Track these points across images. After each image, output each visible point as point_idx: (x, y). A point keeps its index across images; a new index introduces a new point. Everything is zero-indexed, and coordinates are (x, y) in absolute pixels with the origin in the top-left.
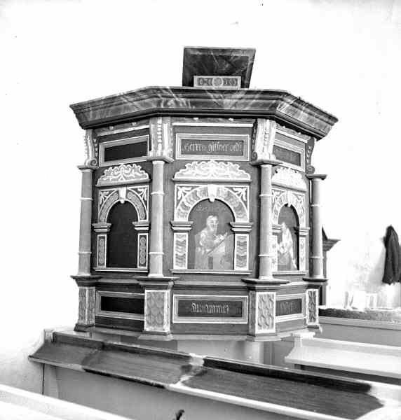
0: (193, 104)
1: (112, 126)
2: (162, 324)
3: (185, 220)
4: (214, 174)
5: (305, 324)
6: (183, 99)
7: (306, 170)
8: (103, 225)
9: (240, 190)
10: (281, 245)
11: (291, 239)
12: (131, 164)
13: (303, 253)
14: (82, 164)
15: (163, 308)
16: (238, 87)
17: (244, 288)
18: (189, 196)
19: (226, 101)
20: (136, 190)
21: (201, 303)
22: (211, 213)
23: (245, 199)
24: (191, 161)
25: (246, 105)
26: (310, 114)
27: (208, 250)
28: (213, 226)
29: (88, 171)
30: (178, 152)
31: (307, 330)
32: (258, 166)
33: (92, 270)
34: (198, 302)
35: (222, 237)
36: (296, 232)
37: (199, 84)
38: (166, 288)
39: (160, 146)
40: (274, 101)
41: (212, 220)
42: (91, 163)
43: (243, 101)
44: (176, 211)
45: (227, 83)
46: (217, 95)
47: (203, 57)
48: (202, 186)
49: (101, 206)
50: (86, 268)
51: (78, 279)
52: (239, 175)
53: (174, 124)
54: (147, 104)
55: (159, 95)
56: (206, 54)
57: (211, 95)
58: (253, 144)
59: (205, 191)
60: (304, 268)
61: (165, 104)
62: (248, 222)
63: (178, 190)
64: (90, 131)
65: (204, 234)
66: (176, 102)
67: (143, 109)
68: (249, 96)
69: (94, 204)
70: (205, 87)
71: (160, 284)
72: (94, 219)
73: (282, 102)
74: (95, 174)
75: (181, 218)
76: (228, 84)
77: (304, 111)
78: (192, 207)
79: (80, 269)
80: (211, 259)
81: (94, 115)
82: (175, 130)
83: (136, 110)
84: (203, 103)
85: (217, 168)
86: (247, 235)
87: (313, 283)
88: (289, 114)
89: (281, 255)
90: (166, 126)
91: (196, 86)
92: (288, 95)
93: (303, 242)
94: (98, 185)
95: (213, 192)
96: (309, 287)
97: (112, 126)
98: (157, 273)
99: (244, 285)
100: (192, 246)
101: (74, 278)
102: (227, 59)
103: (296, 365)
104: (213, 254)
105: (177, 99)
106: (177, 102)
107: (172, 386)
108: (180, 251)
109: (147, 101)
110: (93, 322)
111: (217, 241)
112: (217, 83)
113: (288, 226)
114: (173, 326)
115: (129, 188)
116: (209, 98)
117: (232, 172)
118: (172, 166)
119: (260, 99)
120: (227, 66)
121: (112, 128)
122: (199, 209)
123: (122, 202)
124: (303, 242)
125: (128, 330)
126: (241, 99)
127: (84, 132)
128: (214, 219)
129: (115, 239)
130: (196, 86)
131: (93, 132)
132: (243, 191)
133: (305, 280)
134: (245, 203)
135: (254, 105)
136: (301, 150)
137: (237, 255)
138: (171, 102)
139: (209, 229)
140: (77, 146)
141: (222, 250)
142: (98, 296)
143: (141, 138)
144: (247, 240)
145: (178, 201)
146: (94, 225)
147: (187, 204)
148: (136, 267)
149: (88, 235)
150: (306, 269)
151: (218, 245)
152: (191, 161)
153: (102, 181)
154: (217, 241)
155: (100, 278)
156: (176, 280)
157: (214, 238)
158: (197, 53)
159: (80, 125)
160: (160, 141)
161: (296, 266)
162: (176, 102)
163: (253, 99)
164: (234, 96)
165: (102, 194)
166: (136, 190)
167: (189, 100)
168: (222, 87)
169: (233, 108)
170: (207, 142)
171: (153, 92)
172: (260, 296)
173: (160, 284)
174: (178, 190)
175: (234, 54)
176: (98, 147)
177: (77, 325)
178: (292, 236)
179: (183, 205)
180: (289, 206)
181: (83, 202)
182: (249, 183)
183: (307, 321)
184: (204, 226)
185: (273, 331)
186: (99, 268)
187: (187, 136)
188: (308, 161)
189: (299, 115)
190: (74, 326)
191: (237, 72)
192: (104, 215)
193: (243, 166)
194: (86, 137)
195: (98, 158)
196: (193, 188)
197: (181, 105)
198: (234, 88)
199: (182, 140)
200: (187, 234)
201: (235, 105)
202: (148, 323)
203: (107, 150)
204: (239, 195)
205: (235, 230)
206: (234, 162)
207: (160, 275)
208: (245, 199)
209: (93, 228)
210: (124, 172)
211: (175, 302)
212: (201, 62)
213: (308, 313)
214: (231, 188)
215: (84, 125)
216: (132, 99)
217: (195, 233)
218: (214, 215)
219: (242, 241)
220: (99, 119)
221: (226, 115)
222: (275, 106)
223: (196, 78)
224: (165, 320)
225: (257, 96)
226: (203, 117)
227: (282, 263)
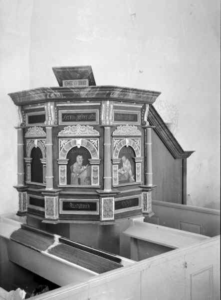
0: (64, 95)
1: (29, 106)
2: (53, 215)
3: (65, 158)
4: (79, 134)
5: (141, 212)
6: (59, 93)
7: (141, 124)
8: (29, 159)
9: (94, 141)
10: (121, 169)
11: (130, 165)
12: (39, 127)
13: (139, 172)
14: (17, 126)
15: (53, 206)
16: (87, 85)
17: (96, 195)
18: (67, 145)
19: (82, 93)
20: (41, 141)
21: (75, 203)
22: (79, 154)
23: (96, 146)
24: (66, 126)
25: (92, 94)
26: (136, 93)
27: (78, 174)
28: (80, 161)
29: (20, 129)
30: (60, 121)
31: (142, 215)
32: (102, 128)
33: (25, 183)
34: (72, 203)
35: (85, 167)
36: (133, 161)
37: (65, 85)
38: (55, 196)
39: (50, 118)
40: (108, 92)
41: (80, 158)
42: (21, 125)
43: (91, 92)
44: (60, 154)
45: (81, 83)
46: (76, 90)
47: (64, 72)
48: (73, 139)
49: (114, 148)
50: (21, 182)
51: (20, 189)
52: (93, 133)
53: (57, 105)
54: (40, 96)
55: (45, 92)
56: (65, 70)
57: (73, 90)
58: (100, 115)
59: (75, 142)
60: (139, 180)
61: (49, 96)
62: (98, 158)
63: (60, 142)
64: (20, 107)
65: (75, 166)
66: (55, 94)
67: (40, 98)
68: (94, 89)
69: (25, 147)
70: (68, 87)
71: (51, 194)
72: (25, 155)
73: (113, 92)
74: (24, 130)
75: (63, 157)
76: (81, 84)
77: (132, 93)
78: (68, 151)
79: (19, 183)
80: (79, 180)
81: (20, 100)
82: (58, 108)
83: (37, 99)
84: (68, 95)
85: (81, 129)
86: (98, 166)
87: (145, 189)
88: (121, 97)
89: (121, 175)
90: (52, 107)
91: (64, 86)
92: (116, 88)
93: (139, 166)
94: (26, 137)
95: (79, 143)
96: (143, 191)
97: (29, 106)
98: (50, 188)
99: (96, 194)
100: (69, 172)
101: (15, 187)
102: (77, 72)
103: (131, 238)
104: (80, 177)
105: (56, 93)
106: (55, 95)
107: (43, 252)
108: (62, 175)
109: (40, 94)
110: (26, 210)
111: (82, 169)
112: (75, 84)
113: (127, 158)
114: (60, 215)
115: (39, 139)
116: (72, 92)
117: (90, 131)
118: (56, 129)
119: (99, 91)
120: (78, 75)
121: (30, 106)
122: (73, 152)
123: (36, 147)
124: (139, 166)
125: (39, 216)
126: (90, 91)
127: (17, 107)
128: (81, 157)
129: (33, 165)
130: (64, 86)
131: (22, 108)
132: (95, 142)
133: (141, 187)
134: (97, 148)
135: (98, 94)
136: (138, 113)
137: (93, 178)
138: (52, 95)
139: (78, 163)
140: (14, 116)
141: (85, 174)
142: (27, 196)
143: (42, 112)
144: (98, 169)
145: (61, 148)
146: (25, 158)
147: (65, 149)
148: (42, 183)
149: (22, 165)
150: (142, 180)
151: (83, 171)
152: (66, 126)
153: (27, 135)
154: (82, 169)
155: (28, 187)
156: (60, 191)
157: (81, 168)
158: (60, 70)
159: (15, 104)
160: (50, 115)
161: (134, 180)
162: (55, 94)
163: (96, 91)
164: (85, 90)
165: (28, 141)
166: (41, 141)
167: (62, 93)
168: (77, 86)
169: (86, 97)
170: (76, 115)
171: (43, 90)
172: (105, 200)
173: (51, 194)
174: (60, 142)
175: (80, 69)
176: (25, 115)
177: (18, 212)
178: (131, 162)
179: (64, 150)
180: (127, 146)
181: (18, 146)
182: (99, 137)
183: (143, 210)
184: (75, 161)
185: (113, 218)
186: (29, 182)
187: (65, 111)
188: (142, 118)
189: (129, 95)
190: (17, 212)
191: (85, 77)
192: (29, 154)
193: (95, 127)
194: (19, 110)
195: (25, 121)
196: (68, 140)
197: (58, 96)
198: (84, 86)
199: (63, 114)
200: (66, 166)
201: (87, 95)
202: (47, 214)
203: (30, 117)
204: (93, 144)
205: (91, 163)
206: (90, 125)
207: (51, 189)
208: (96, 146)
209: (24, 160)
210: (35, 131)
211: (61, 203)
212: (63, 74)
213: (142, 205)
214: (89, 140)
215: (16, 104)
216: (34, 93)
217: (70, 165)
218: (80, 155)
219: (96, 169)
220: (22, 101)
221: (85, 100)
222: (110, 94)
223: (64, 82)
224: (54, 213)
225: (98, 89)
226: (72, 100)
227: (122, 179)
